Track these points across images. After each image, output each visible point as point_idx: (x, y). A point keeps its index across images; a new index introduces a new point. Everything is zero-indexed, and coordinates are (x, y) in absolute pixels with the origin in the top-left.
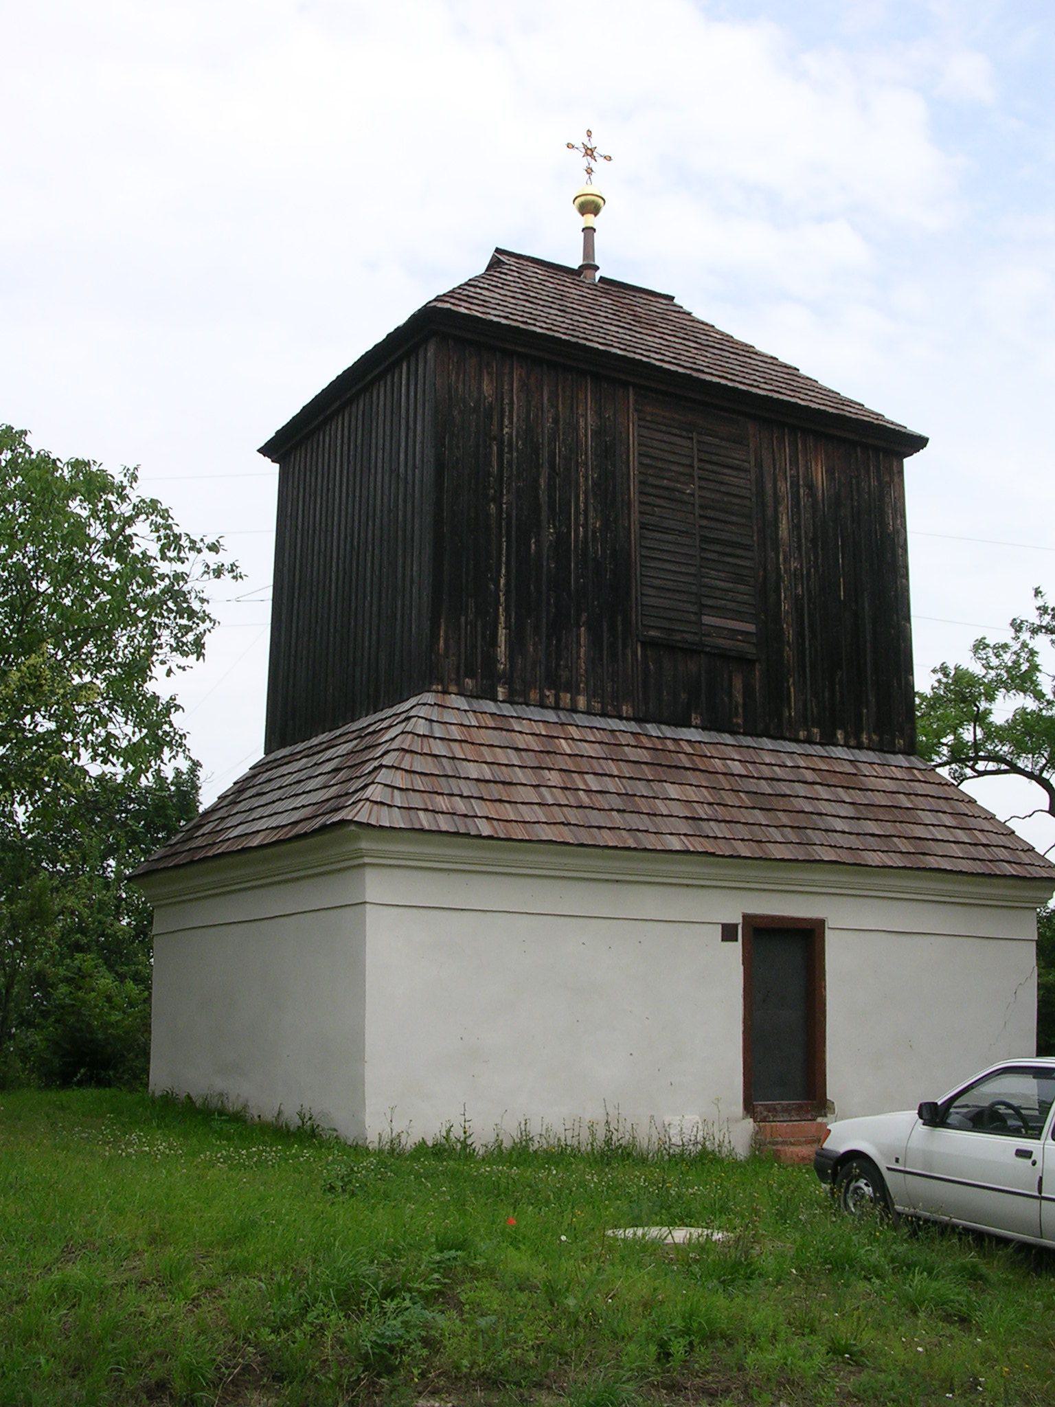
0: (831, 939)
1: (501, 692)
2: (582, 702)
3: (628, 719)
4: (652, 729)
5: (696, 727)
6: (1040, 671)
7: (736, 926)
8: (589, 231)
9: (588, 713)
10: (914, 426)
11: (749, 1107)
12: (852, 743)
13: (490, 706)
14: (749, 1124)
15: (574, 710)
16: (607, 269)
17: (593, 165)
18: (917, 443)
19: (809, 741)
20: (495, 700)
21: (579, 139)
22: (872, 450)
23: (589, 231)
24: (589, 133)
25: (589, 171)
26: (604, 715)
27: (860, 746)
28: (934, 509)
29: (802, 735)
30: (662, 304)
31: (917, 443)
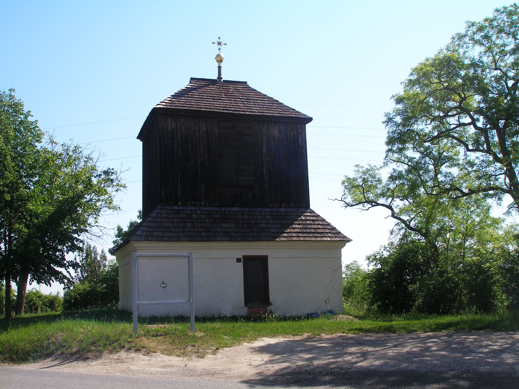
0: (270, 260)
1: (180, 203)
2: (203, 203)
3: (216, 207)
4: (223, 209)
5: (237, 207)
6: (120, 229)
7: (241, 259)
8: (220, 68)
9: (205, 206)
10: (309, 115)
11: (246, 303)
12: (288, 206)
13: (176, 208)
14: (246, 308)
16: (225, 77)
17: (221, 47)
18: (310, 120)
19: (273, 207)
20: (178, 206)
21: (216, 40)
22: (298, 122)
23: (220, 68)
24: (219, 38)
25: (219, 49)
26: (209, 206)
27: (290, 207)
28: (314, 136)
29: (271, 206)
30: (240, 87)
31: (310, 120)
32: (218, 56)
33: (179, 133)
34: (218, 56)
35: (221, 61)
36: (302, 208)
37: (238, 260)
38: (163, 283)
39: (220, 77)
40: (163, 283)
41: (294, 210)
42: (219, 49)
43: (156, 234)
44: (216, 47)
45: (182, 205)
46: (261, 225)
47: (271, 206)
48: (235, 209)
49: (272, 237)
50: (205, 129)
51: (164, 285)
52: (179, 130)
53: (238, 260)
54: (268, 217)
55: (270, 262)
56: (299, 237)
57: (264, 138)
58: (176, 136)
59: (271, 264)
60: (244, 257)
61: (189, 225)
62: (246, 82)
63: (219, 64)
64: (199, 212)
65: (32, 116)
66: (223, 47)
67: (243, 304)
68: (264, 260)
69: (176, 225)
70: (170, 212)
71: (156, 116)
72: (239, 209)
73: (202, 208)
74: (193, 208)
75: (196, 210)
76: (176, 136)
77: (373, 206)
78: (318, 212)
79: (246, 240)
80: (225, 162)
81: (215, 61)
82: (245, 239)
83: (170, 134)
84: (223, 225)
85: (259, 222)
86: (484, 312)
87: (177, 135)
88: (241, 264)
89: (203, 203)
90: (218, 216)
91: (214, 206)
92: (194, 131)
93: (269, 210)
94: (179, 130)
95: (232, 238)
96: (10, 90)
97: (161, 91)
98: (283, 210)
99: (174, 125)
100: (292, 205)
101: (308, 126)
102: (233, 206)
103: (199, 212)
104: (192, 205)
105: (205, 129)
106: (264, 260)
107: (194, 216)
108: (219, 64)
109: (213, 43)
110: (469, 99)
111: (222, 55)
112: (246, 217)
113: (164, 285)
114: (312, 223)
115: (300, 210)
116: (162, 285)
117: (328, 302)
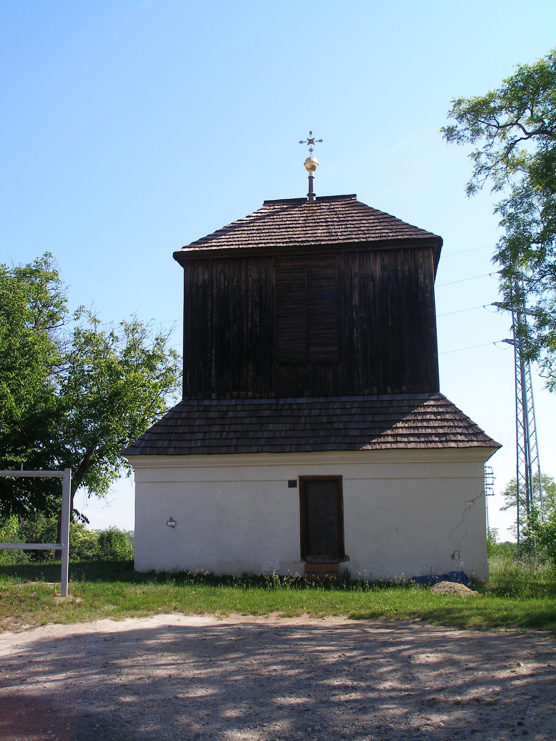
2: (250, 393)
3: (272, 398)
5: (307, 396)
7: (295, 481)
8: (311, 178)
9: (254, 398)
13: (207, 402)
15: (247, 397)
16: (319, 192)
19: (371, 394)
23: (311, 178)
25: (311, 150)
26: (261, 398)
27: (401, 392)
32: (309, 160)
33: (214, 287)
34: (309, 160)
35: (313, 168)
36: (424, 393)
37: (292, 484)
38: (171, 520)
39: (311, 194)
40: (171, 520)
41: (407, 397)
42: (311, 150)
43: (160, 444)
44: (306, 147)
45: (218, 399)
47: (366, 392)
48: (301, 400)
49: (352, 444)
50: (255, 276)
51: (173, 523)
52: (215, 282)
53: (292, 484)
55: (347, 486)
56: (397, 442)
57: (356, 280)
58: (209, 292)
59: (349, 490)
60: (302, 478)
62: (355, 195)
63: (310, 173)
65: (507, 341)
66: (316, 146)
67: (298, 557)
68: (336, 482)
72: (310, 400)
73: (247, 402)
74: (233, 402)
76: (209, 292)
78: (451, 397)
79: (298, 451)
81: (304, 168)
82: (299, 447)
83: (201, 290)
85: (335, 419)
86: (381, 588)
87: (212, 291)
88: (296, 492)
89: (250, 393)
91: (268, 398)
92: (238, 281)
93: (361, 399)
94: (215, 282)
95: (276, 446)
96: (46, 255)
98: (386, 397)
99: (206, 276)
100: (404, 388)
102: (301, 395)
104: (232, 398)
106: (336, 482)
107: (230, 414)
108: (310, 173)
109: (301, 142)
111: (315, 160)
112: (315, 412)
113: (173, 523)
114: (433, 417)
115: (420, 396)
116: (169, 523)
117: (456, 557)
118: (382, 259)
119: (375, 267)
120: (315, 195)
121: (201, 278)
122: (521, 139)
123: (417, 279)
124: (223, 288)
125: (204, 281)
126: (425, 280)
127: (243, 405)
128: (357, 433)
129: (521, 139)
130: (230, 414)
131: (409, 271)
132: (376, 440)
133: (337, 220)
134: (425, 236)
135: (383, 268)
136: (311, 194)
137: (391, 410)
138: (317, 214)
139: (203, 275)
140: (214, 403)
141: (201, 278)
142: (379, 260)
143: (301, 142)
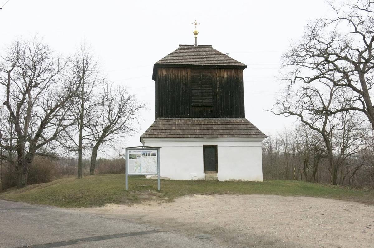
7: (205, 147)
8: (196, 38)
10: (245, 64)
13: (168, 118)
16: (199, 43)
23: (196, 38)
31: (246, 67)
39: (196, 44)
42: (196, 27)
46: (214, 128)
48: (200, 119)
54: (219, 123)
61: (174, 128)
62: (211, 46)
64: (180, 121)
68: (215, 147)
69: (166, 128)
70: (164, 121)
71: (157, 67)
75: (178, 120)
77: (291, 115)
80: (199, 92)
83: (164, 78)
84: (192, 128)
90: (190, 123)
97: (163, 50)
101: (245, 71)
103: (180, 121)
105: (184, 74)
106: (215, 147)
107: (177, 123)
110: (64, 121)
112: (206, 123)
118: (227, 71)
119: (225, 74)
120: (197, 44)
121: (164, 74)
122: (329, 86)
123: (238, 79)
124: (172, 78)
125: (165, 75)
126: (241, 79)
127: (181, 120)
128: (222, 131)
129: (329, 86)
130: (177, 123)
131: (236, 76)
132: (115, 128)
133: (224, 61)
134: (241, 65)
135: (227, 74)
136: (196, 44)
137: (231, 123)
138: (215, 60)
139: (164, 73)
140: (170, 119)
141: (164, 74)
142: (226, 72)
143: (192, 24)
